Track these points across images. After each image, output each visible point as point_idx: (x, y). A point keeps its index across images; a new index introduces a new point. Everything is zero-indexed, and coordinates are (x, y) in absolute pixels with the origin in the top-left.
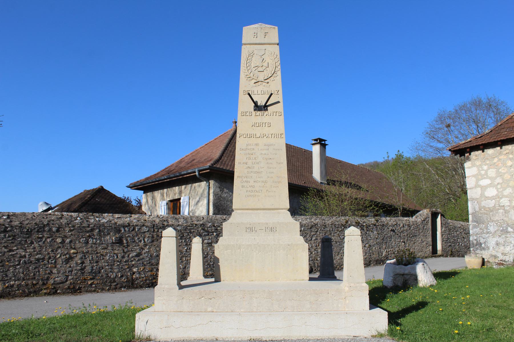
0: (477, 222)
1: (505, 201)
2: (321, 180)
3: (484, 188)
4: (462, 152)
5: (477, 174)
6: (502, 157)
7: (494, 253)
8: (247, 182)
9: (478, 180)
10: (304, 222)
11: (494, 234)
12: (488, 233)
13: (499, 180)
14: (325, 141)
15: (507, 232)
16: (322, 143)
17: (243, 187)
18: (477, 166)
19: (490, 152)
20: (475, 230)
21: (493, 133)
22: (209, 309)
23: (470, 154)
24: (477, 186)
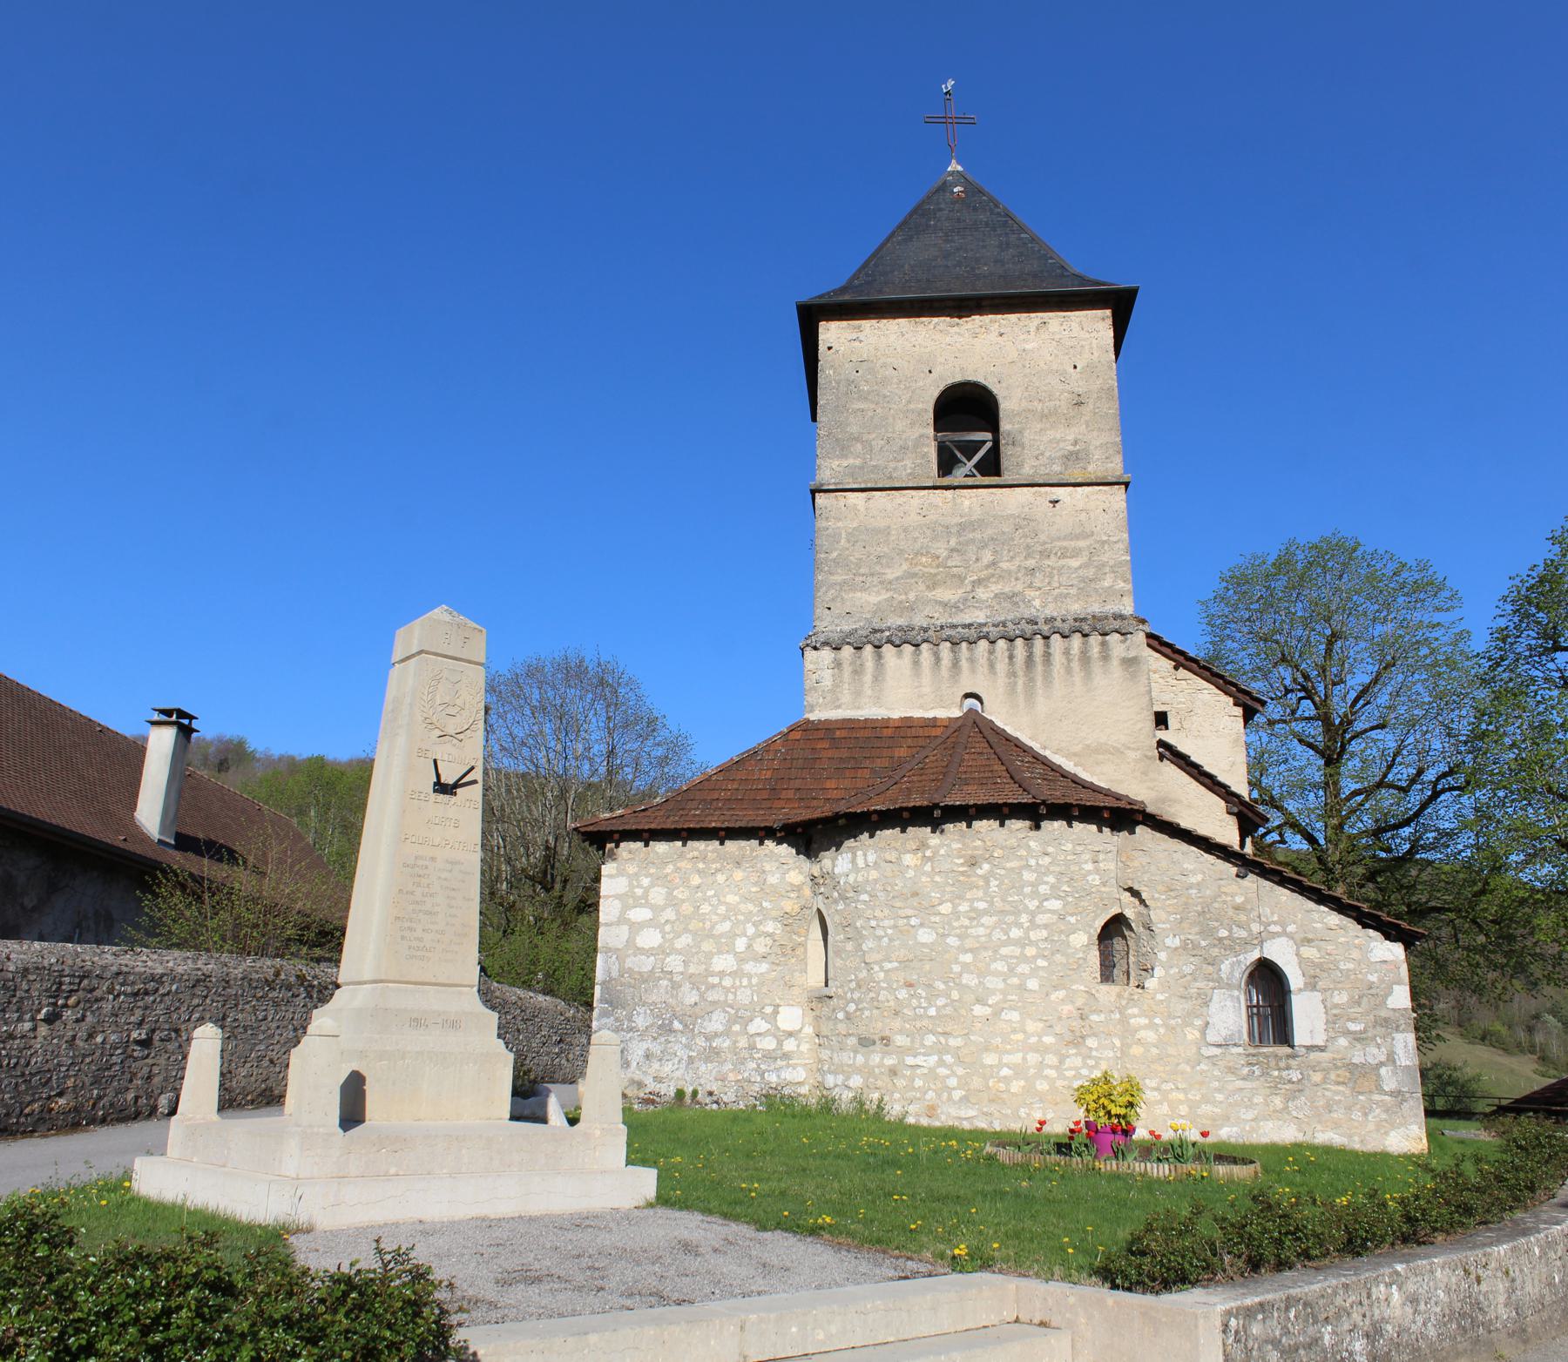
0: (610, 1003)
1: (674, 963)
2: (161, 833)
3: (636, 928)
4: (601, 840)
5: (625, 894)
6: (683, 864)
7: (638, 1076)
8: (410, 929)
9: (626, 908)
10: (180, 970)
11: (643, 1035)
12: (631, 1029)
13: (669, 914)
14: (191, 718)
15: (671, 1031)
16: (182, 723)
17: (403, 938)
18: (629, 876)
19: (661, 847)
20: (605, 1020)
21: (671, 805)
22: (393, 1171)
23: (617, 846)
24: (622, 920)
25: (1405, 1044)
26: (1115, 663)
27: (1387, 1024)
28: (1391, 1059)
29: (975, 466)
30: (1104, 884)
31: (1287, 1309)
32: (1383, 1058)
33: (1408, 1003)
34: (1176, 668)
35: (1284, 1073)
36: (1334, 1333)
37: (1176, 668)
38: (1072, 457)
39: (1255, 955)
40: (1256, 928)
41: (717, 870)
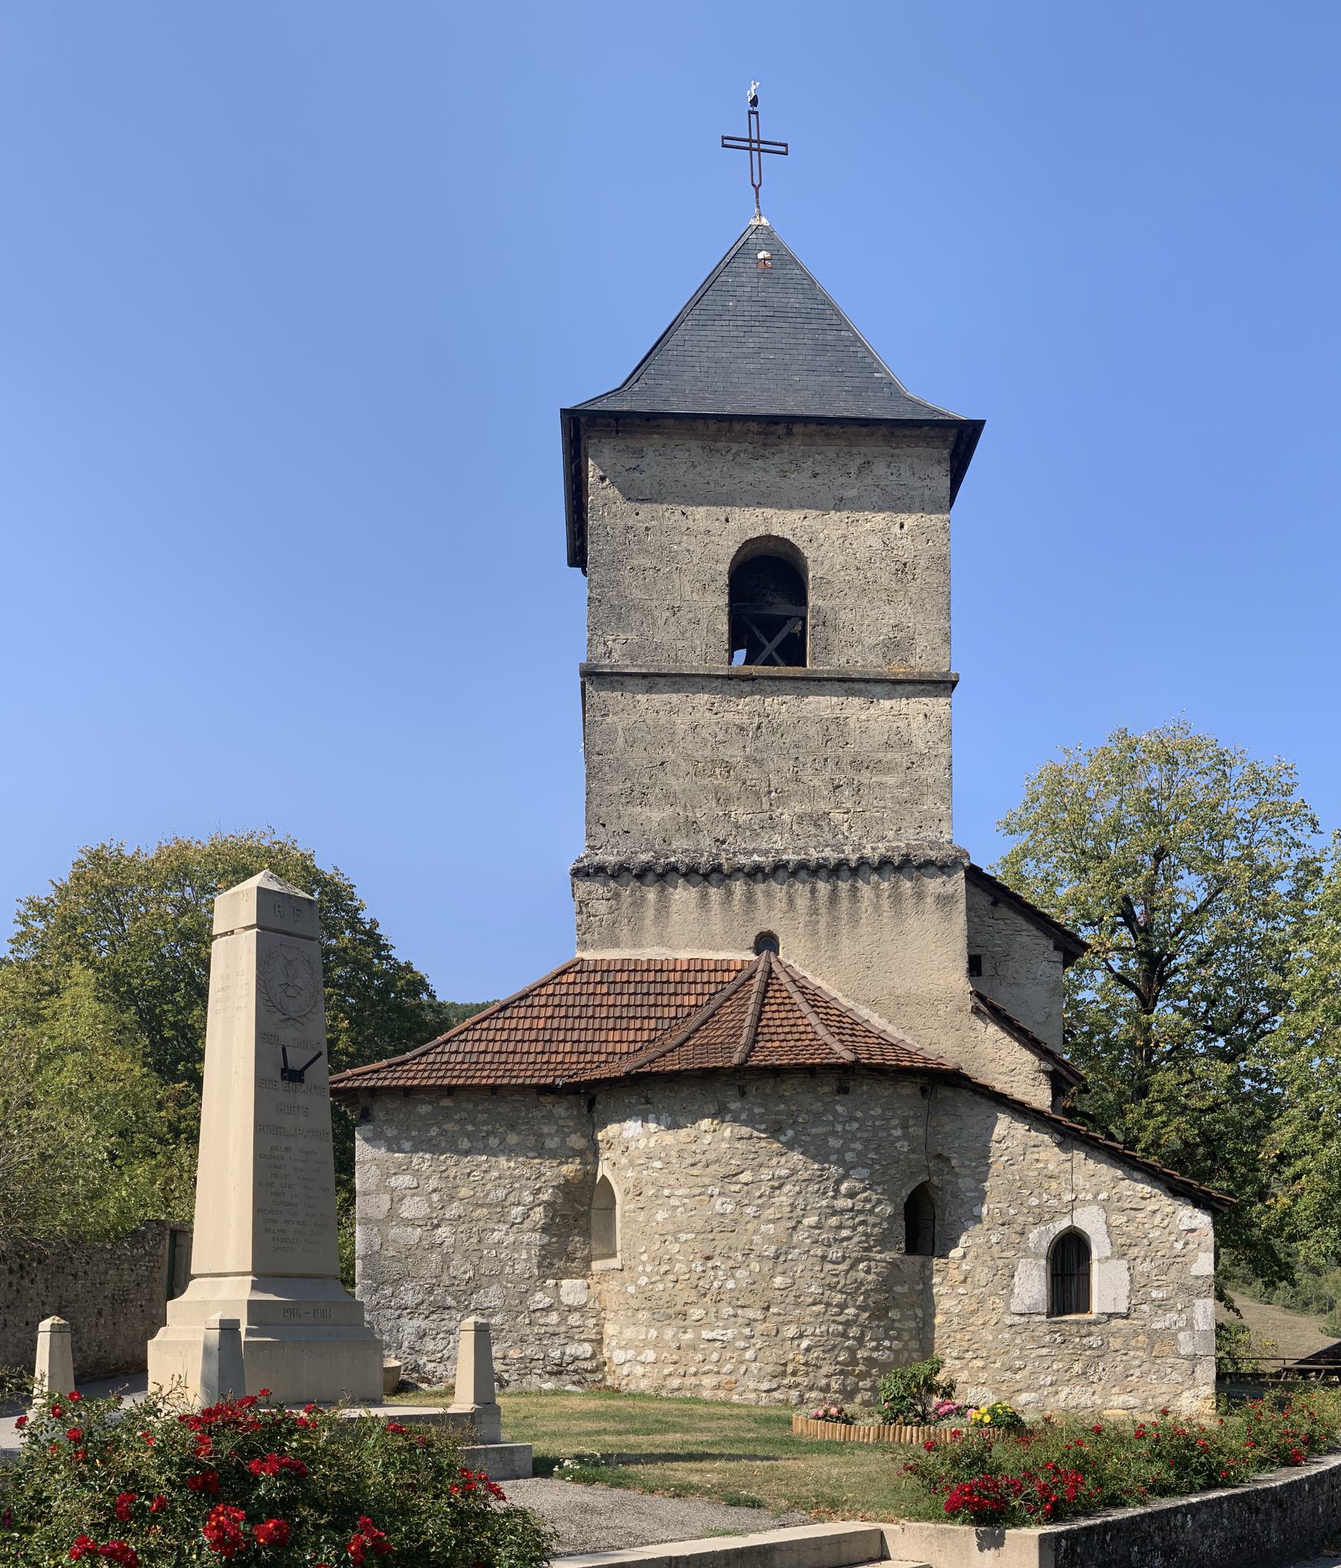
8: (274, 1221)
25: (1205, 1311)
26: (929, 900)
27: (1189, 1291)
28: (1190, 1325)
29: (776, 650)
30: (913, 1151)
31: (1105, 1534)
32: (1181, 1324)
34: (995, 904)
35: (1085, 1341)
36: (1139, 1552)
37: (995, 904)
38: (897, 645)
39: (1064, 1224)
40: (1068, 1197)
41: (489, 1133)
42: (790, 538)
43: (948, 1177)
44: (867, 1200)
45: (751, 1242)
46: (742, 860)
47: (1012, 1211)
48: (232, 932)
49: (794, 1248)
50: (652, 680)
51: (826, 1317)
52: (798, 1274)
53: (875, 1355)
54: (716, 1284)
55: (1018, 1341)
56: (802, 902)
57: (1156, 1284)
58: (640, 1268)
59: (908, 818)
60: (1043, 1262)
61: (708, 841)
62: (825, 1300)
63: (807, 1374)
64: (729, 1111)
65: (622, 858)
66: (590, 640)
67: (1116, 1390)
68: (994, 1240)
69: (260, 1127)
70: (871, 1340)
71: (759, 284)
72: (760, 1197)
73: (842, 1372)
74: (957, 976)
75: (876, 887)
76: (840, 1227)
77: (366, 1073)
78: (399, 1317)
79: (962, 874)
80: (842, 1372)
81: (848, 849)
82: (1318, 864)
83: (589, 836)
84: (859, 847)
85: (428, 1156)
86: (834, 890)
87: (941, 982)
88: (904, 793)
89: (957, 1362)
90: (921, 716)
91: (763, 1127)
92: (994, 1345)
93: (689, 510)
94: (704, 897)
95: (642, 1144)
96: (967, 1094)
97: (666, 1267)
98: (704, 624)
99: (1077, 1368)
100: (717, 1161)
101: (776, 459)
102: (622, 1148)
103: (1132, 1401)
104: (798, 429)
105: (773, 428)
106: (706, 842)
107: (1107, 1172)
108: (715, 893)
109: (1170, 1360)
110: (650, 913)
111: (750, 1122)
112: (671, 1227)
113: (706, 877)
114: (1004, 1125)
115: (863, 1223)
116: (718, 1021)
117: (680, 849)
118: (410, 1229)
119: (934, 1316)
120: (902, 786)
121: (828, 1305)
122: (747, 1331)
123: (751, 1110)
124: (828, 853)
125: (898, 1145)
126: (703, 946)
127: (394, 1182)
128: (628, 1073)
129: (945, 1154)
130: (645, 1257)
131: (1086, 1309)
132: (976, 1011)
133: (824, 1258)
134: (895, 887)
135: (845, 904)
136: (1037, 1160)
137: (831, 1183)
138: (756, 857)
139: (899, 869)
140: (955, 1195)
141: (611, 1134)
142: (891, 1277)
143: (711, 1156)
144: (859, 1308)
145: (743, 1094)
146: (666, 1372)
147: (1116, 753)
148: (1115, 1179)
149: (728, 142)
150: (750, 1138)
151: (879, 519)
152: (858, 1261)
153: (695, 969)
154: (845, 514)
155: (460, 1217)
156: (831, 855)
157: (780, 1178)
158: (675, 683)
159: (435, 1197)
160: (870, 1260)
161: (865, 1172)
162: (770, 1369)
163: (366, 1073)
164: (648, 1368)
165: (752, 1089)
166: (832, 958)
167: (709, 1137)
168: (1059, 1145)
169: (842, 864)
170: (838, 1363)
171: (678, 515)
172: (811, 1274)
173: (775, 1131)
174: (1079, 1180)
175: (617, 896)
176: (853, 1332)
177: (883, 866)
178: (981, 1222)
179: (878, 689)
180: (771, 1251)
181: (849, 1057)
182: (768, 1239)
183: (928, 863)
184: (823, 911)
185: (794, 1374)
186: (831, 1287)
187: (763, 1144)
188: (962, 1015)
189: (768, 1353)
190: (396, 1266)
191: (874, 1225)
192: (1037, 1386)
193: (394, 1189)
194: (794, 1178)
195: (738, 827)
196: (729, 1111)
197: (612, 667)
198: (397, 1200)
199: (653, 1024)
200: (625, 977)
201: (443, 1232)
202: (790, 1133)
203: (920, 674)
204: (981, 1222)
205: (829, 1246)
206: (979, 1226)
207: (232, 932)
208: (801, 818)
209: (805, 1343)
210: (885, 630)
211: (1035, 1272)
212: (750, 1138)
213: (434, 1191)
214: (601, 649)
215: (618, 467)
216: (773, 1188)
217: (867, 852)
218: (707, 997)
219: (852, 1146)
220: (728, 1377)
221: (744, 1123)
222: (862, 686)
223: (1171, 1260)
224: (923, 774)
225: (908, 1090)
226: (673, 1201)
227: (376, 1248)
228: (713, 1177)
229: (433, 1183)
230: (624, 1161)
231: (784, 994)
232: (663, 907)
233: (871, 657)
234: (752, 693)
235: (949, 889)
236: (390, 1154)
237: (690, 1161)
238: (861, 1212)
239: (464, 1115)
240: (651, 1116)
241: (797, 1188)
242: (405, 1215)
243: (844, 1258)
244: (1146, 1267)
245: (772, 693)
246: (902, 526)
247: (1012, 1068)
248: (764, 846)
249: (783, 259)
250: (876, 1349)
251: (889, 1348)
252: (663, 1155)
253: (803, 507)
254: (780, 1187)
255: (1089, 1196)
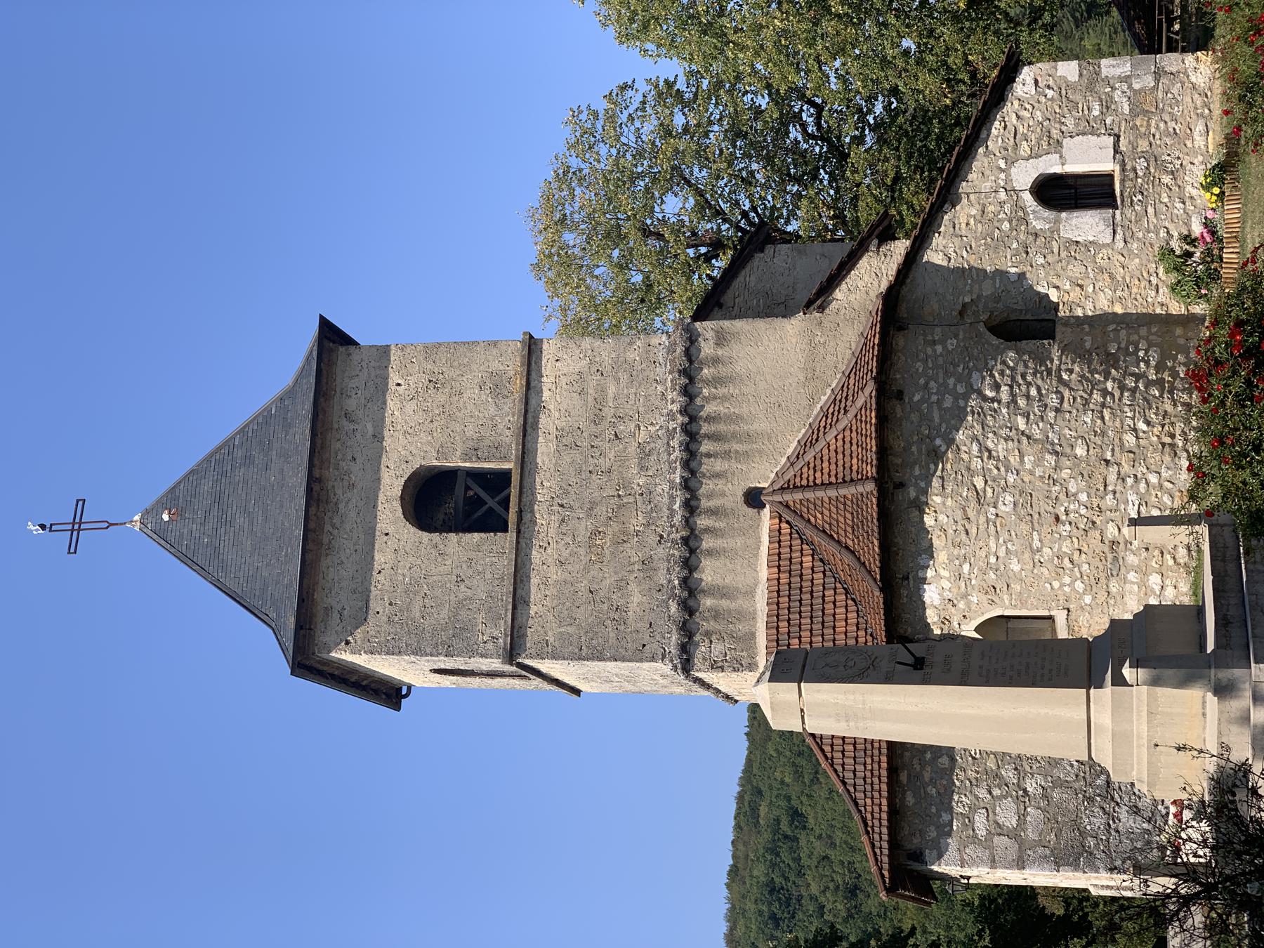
26: (720, 352)
27: (1092, 82)
28: (1126, 79)
30: (956, 336)
32: (1125, 87)
33: (1075, 64)
35: (1140, 174)
37: (720, 306)
38: (497, 388)
39: (1027, 197)
40: (1002, 195)
42: (403, 480)
43: (981, 306)
44: (1002, 373)
45: (1042, 477)
46: (678, 519)
47: (1015, 245)
48: (802, 710)
49: (1048, 437)
50: (519, 601)
51: (1116, 407)
52: (1074, 434)
53: (1153, 363)
54: (1083, 511)
55: (1140, 235)
56: (718, 465)
57: (1086, 112)
58: (1067, 589)
59: (646, 374)
60: (1064, 215)
61: (660, 550)
62: (1099, 408)
63: (1172, 424)
64: (917, 498)
65: (674, 628)
66: (482, 656)
67: (1189, 144)
68: (1041, 260)
69: (963, 681)
70: (1138, 366)
71: (193, 521)
72: (998, 469)
73: (1171, 392)
74: (789, 327)
75: (707, 399)
76: (1028, 397)
77: (875, 854)
78: (1117, 831)
79: (698, 324)
80: (1171, 392)
81: (672, 425)
82: (661, 83)
83: (653, 659)
84: (671, 416)
85: (956, 797)
86: (709, 437)
87: (794, 341)
88: (624, 377)
89: (1161, 291)
90: (558, 364)
91: (932, 466)
92: (1144, 257)
93: (377, 567)
94: (710, 553)
95: (946, 585)
96: (905, 290)
97: (1066, 560)
98: (473, 555)
99: (1167, 179)
100: (964, 510)
101: (339, 492)
102: (950, 606)
103: (1200, 127)
104: (317, 473)
105: (315, 494)
106: (661, 552)
107: (980, 162)
108: (707, 543)
109: (1160, 95)
110: (725, 603)
111: (928, 479)
112: (1027, 555)
113: (692, 551)
114: (934, 256)
115: (1023, 376)
116: (830, 524)
117: (668, 576)
118: (1029, 818)
119: (1115, 314)
120: (617, 379)
121: (1103, 405)
122: (1130, 481)
123: (917, 478)
124: (675, 443)
125: (950, 348)
126: (756, 555)
127: (981, 832)
128: (881, 590)
129: (959, 307)
130: (1056, 584)
131: (1110, 176)
132: (821, 309)
133: (1057, 410)
134: (707, 382)
135: (722, 428)
136: (967, 224)
137: (986, 405)
138: (676, 506)
139: (691, 380)
140: (998, 299)
141: (936, 619)
142: (1077, 351)
143: (959, 513)
144: (1106, 379)
145: (901, 485)
146: (1171, 562)
147: (551, 274)
148: (986, 155)
149: (72, 550)
150: (942, 478)
151: (392, 404)
152: (1060, 379)
153: (777, 561)
154: (386, 433)
155: (1016, 769)
156: (679, 437)
157: (980, 451)
158: (522, 581)
159: (996, 792)
160: (1059, 370)
161: (975, 375)
162: (1167, 459)
163: (875, 854)
164: (1168, 582)
165: (897, 477)
166: (769, 438)
167: (942, 517)
168: (954, 206)
169: (685, 429)
170: (1161, 396)
171: (381, 578)
172: (1073, 422)
173: (936, 456)
174: (987, 186)
175: (708, 634)
176: (1130, 382)
177: (688, 393)
178: (1024, 274)
179: (533, 402)
180: (1050, 459)
181: (871, 387)
182: (1039, 462)
183: (687, 352)
184: (726, 446)
185: (1172, 436)
186: (1086, 403)
187: (948, 466)
188: (826, 323)
189: (1152, 461)
190: (1067, 833)
191: (1026, 366)
192: (1185, 216)
193: (989, 832)
194: (981, 438)
195: (649, 524)
196: (917, 498)
197: (506, 635)
198: (999, 829)
199: (829, 593)
200: (784, 624)
201: (1031, 786)
202: (938, 442)
203: (522, 365)
204: (1024, 274)
205: (1046, 406)
206: (1028, 275)
207: (802, 710)
208: (643, 468)
209: (1142, 426)
210: (484, 397)
211: (1074, 222)
212: (942, 478)
213: (990, 793)
214: (490, 646)
215: (339, 629)
216: (990, 457)
217: (675, 408)
218: (805, 547)
219: (951, 387)
220: (1177, 499)
221: (929, 483)
222: (530, 415)
223: (1064, 100)
224: (608, 361)
225: (900, 340)
226: (1002, 553)
227: (1048, 852)
228: (979, 512)
229: (982, 793)
230: (962, 605)
231: (805, 469)
232: (722, 592)
233: (506, 408)
234: (532, 512)
235: (710, 335)
236: (954, 834)
237: (963, 535)
238: (1013, 378)
239: (915, 761)
240: (920, 575)
241: (990, 435)
242: (1014, 823)
243: (1057, 392)
244: (1070, 122)
245: (533, 494)
246: (399, 385)
247: (874, 272)
248: (666, 500)
249: (170, 499)
250: (1147, 363)
251: (1147, 351)
252: (957, 563)
253: (379, 469)
254: (990, 451)
255: (1002, 176)
